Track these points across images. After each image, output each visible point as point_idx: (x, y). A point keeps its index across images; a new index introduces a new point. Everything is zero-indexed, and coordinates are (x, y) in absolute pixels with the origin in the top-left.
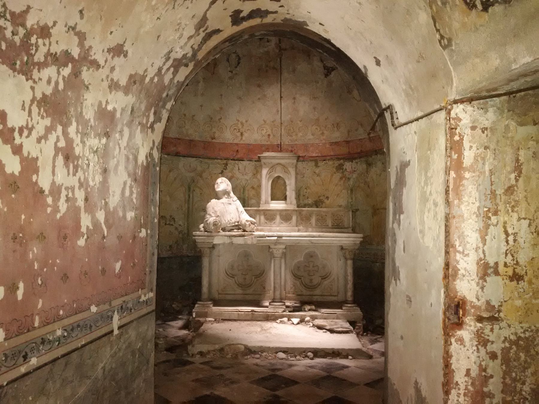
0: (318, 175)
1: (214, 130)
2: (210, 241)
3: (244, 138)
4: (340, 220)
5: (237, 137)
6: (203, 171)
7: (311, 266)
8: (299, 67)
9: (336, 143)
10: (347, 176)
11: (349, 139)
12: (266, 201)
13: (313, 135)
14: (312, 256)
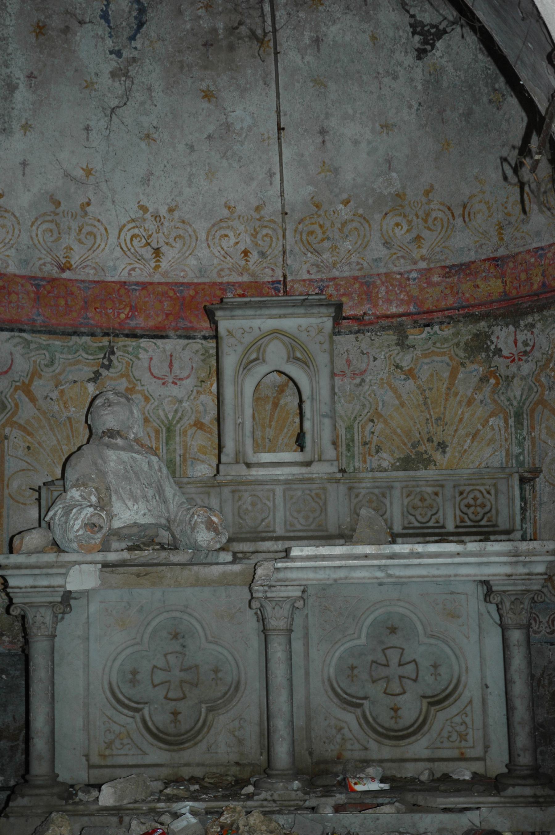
0: (410, 374)
1: (69, 240)
2: (57, 581)
3: (164, 264)
4: (483, 506)
5: (140, 258)
6: (35, 374)
7: (394, 661)
8: (333, 30)
9: (465, 269)
10: (503, 371)
11: (502, 252)
12: (237, 453)
13: (387, 244)
14: (393, 630)
